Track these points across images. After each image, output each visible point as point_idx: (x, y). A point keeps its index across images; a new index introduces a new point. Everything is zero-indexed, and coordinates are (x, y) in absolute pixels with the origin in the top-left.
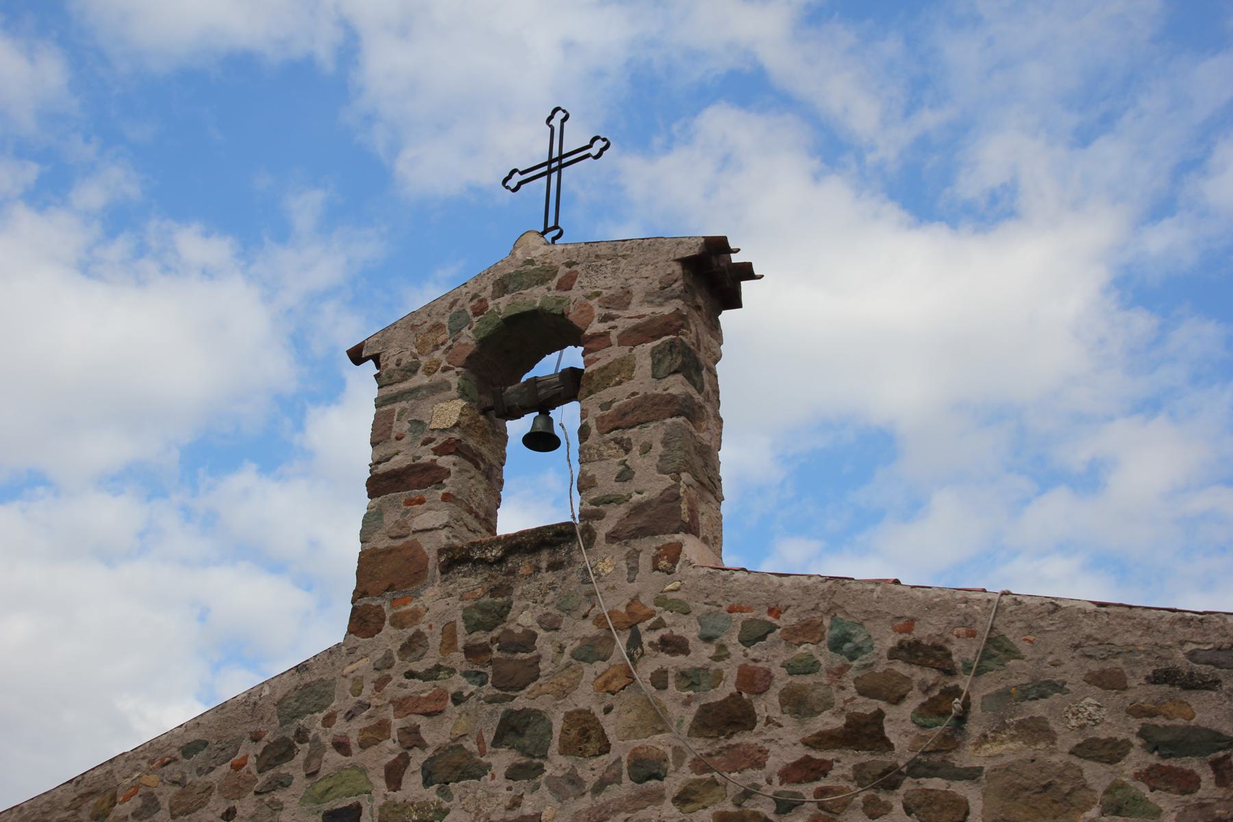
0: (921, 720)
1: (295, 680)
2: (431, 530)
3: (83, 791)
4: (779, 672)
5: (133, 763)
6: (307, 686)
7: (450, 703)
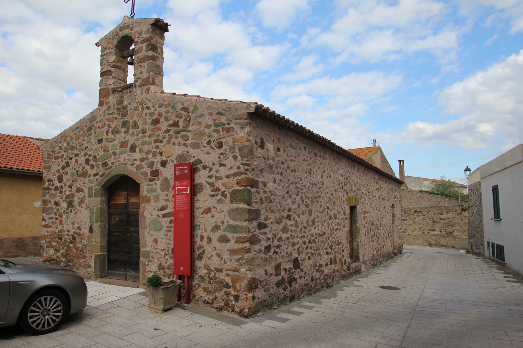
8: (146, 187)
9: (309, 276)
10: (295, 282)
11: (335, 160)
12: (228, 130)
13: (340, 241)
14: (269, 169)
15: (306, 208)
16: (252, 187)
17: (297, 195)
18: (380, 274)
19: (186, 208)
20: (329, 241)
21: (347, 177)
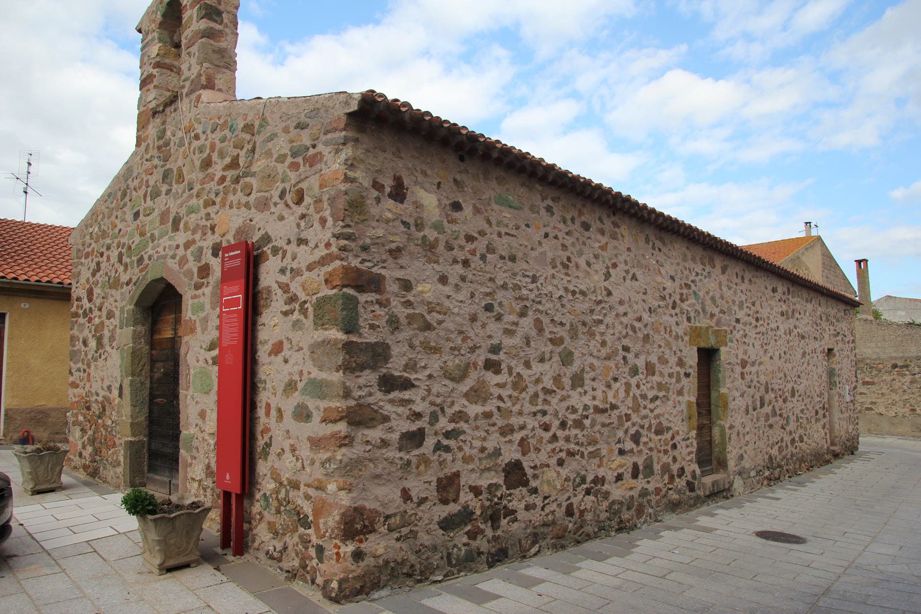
4: (217, 142)
8: (190, 302)
9: (559, 505)
10: (508, 518)
11: (651, 243)
12: (312, 161)
13: (665, 424)
14: (421, 250)
15: (550, 347)
16: (360, 289)
17: (523, 314)
18: (778, 499)
19: (235, 342)
20: (629, 423)
21: (689, 283)
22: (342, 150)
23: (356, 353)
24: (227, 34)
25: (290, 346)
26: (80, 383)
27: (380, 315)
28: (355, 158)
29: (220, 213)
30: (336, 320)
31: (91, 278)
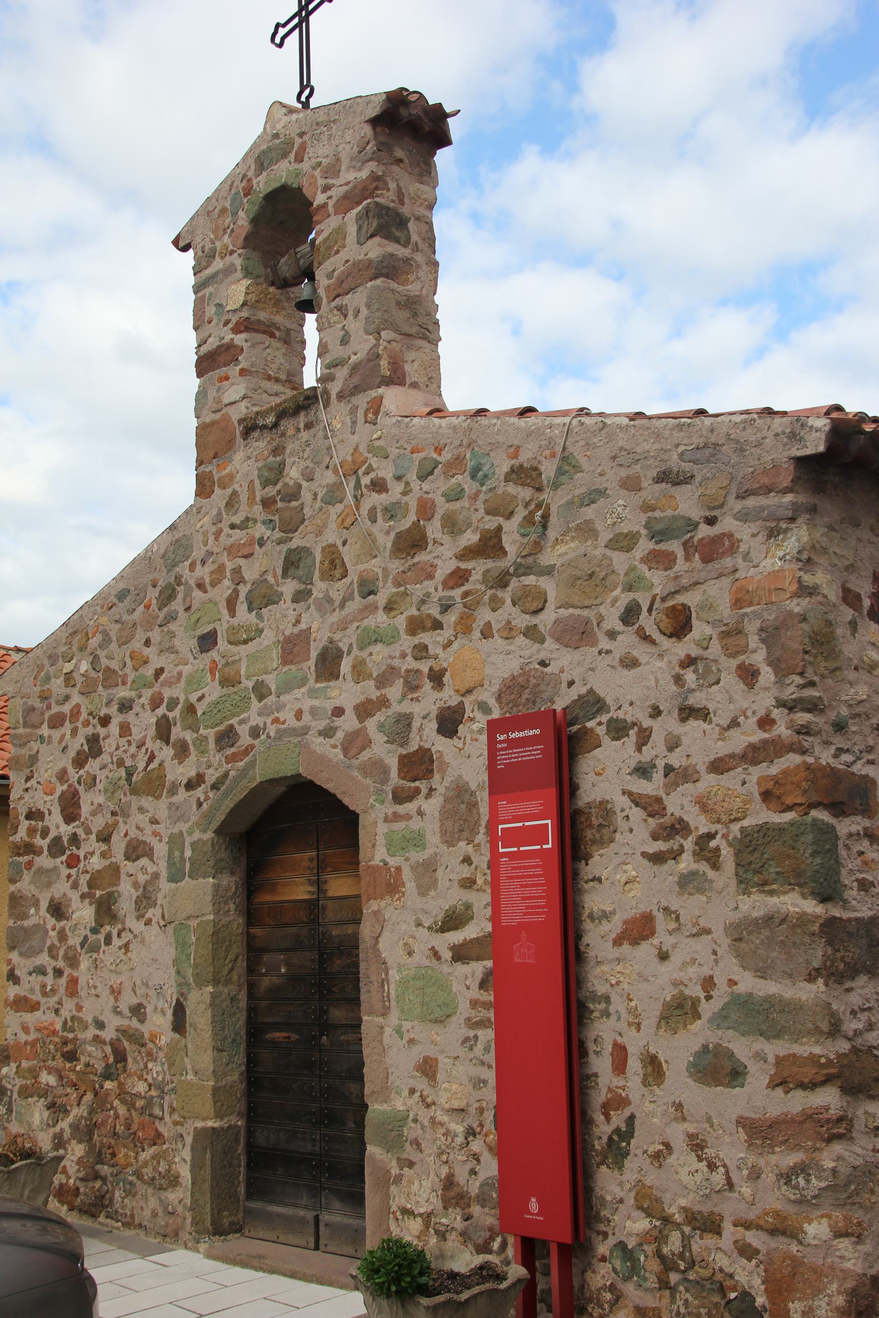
0: (522, 531)
1: (169, 538)
2: (235, 403)
3: (71, 631)
4: (440, 501)
5: (92, 609)
6: (177, 541)
7: (257, 547)
8: (382, 828)
16: (839, 809)
19: (541, 918)
22: (786, 531)
23: (843, 941)
24: (418, 266)
25: (673, 925)
26: (43, 1000)
27: (873, 860)
28: (813, 547)
29: (455, 646)
30: (798, 875)
31: (71, 770)
